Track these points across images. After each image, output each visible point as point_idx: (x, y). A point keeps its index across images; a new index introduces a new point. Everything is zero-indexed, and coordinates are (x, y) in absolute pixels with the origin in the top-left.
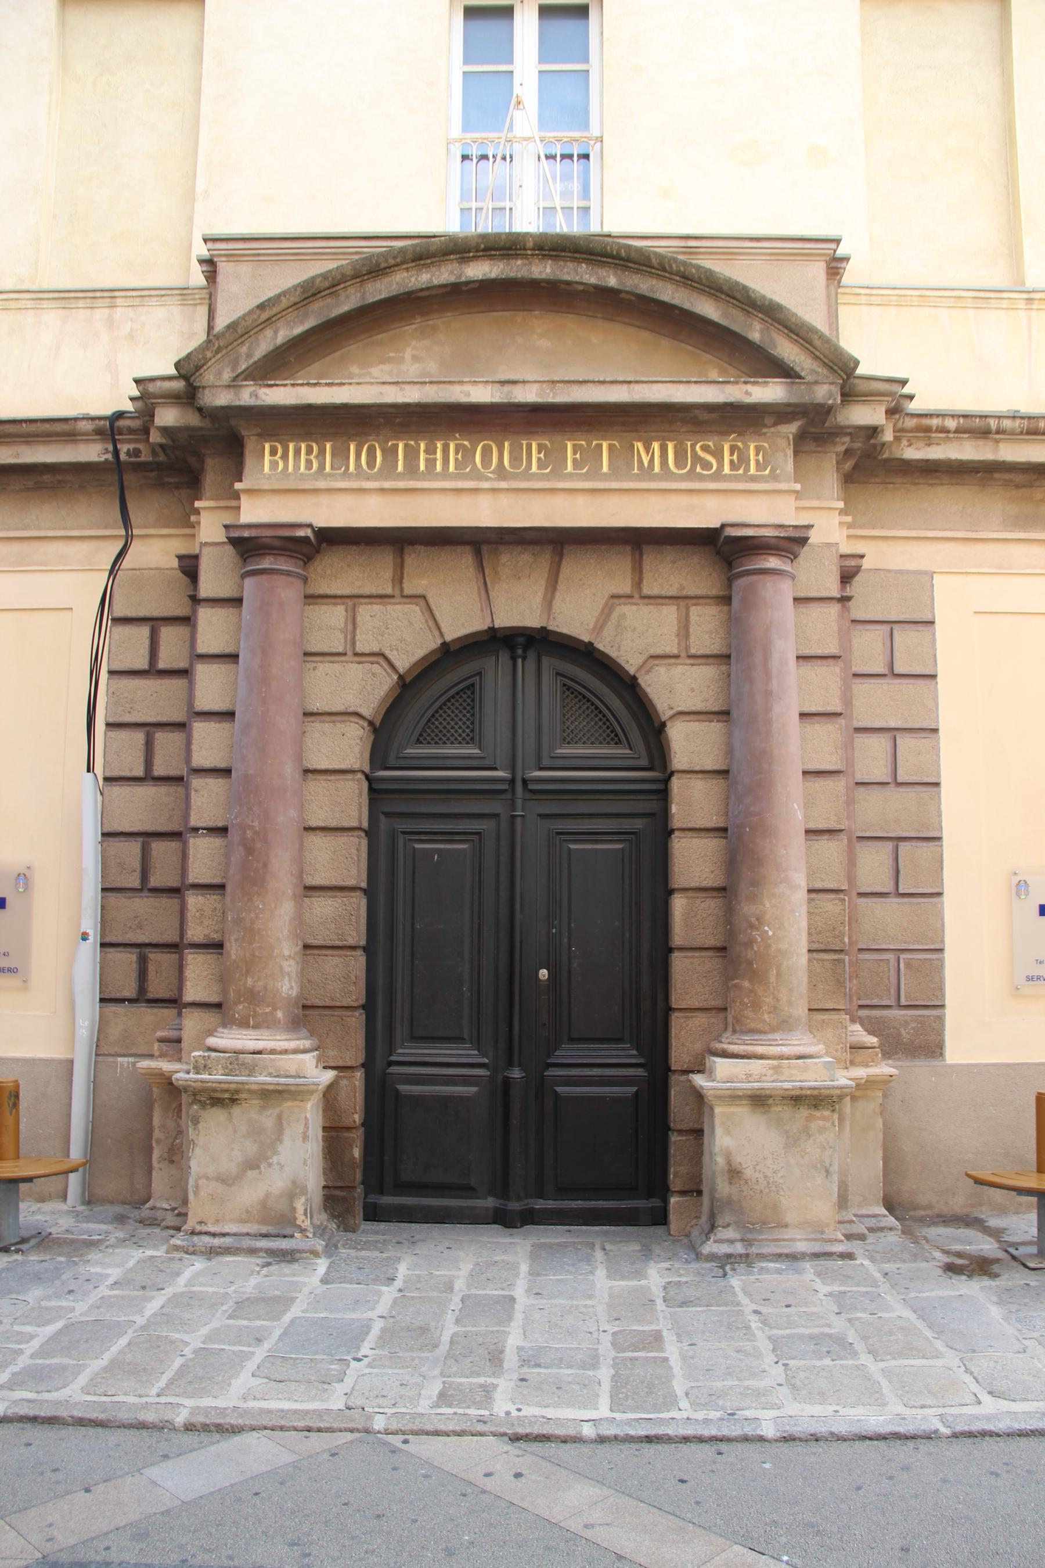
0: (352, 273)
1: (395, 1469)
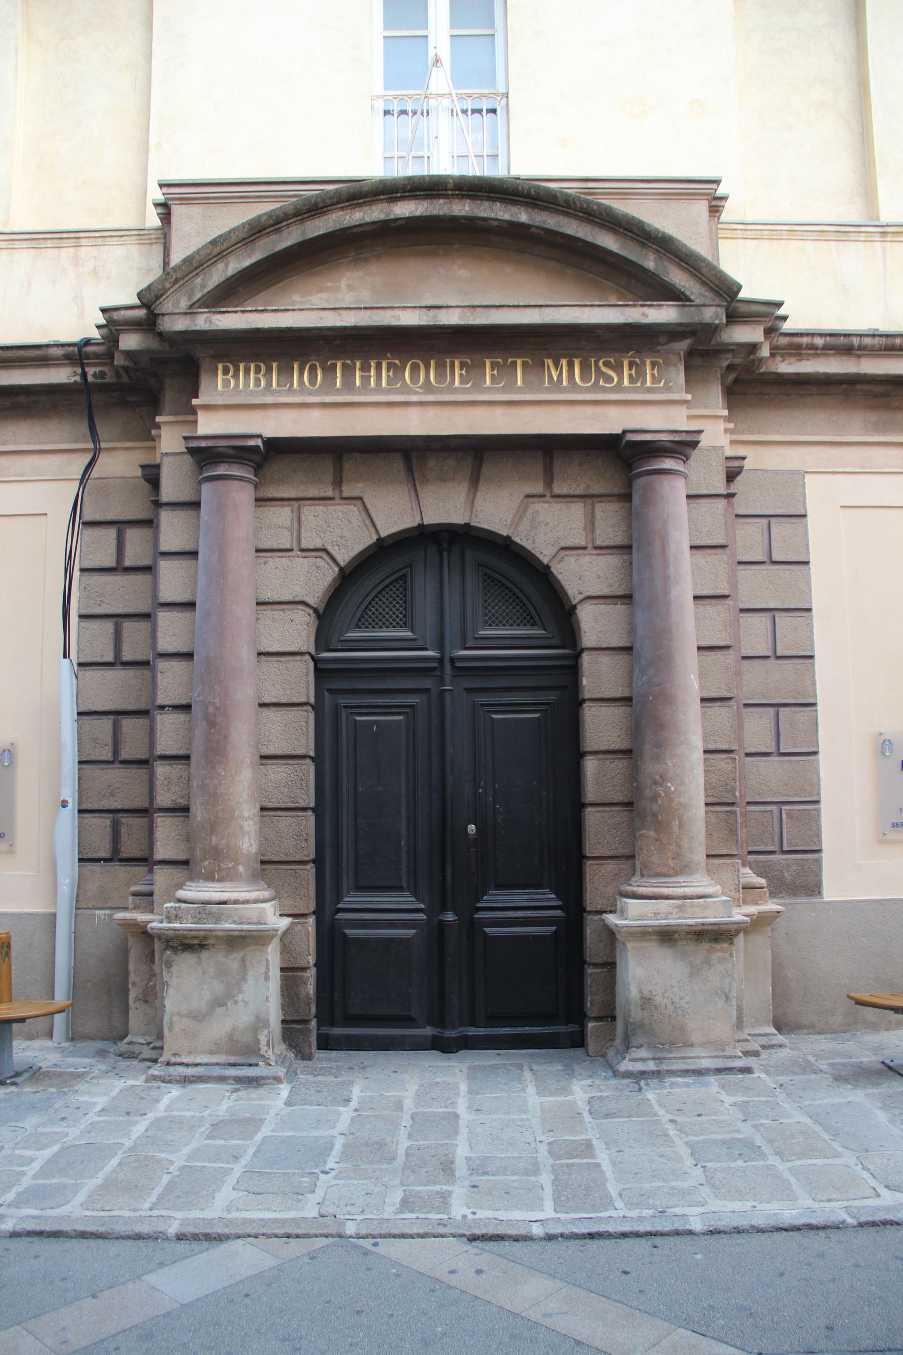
0: (294, 211)
1: (368, 1269)
